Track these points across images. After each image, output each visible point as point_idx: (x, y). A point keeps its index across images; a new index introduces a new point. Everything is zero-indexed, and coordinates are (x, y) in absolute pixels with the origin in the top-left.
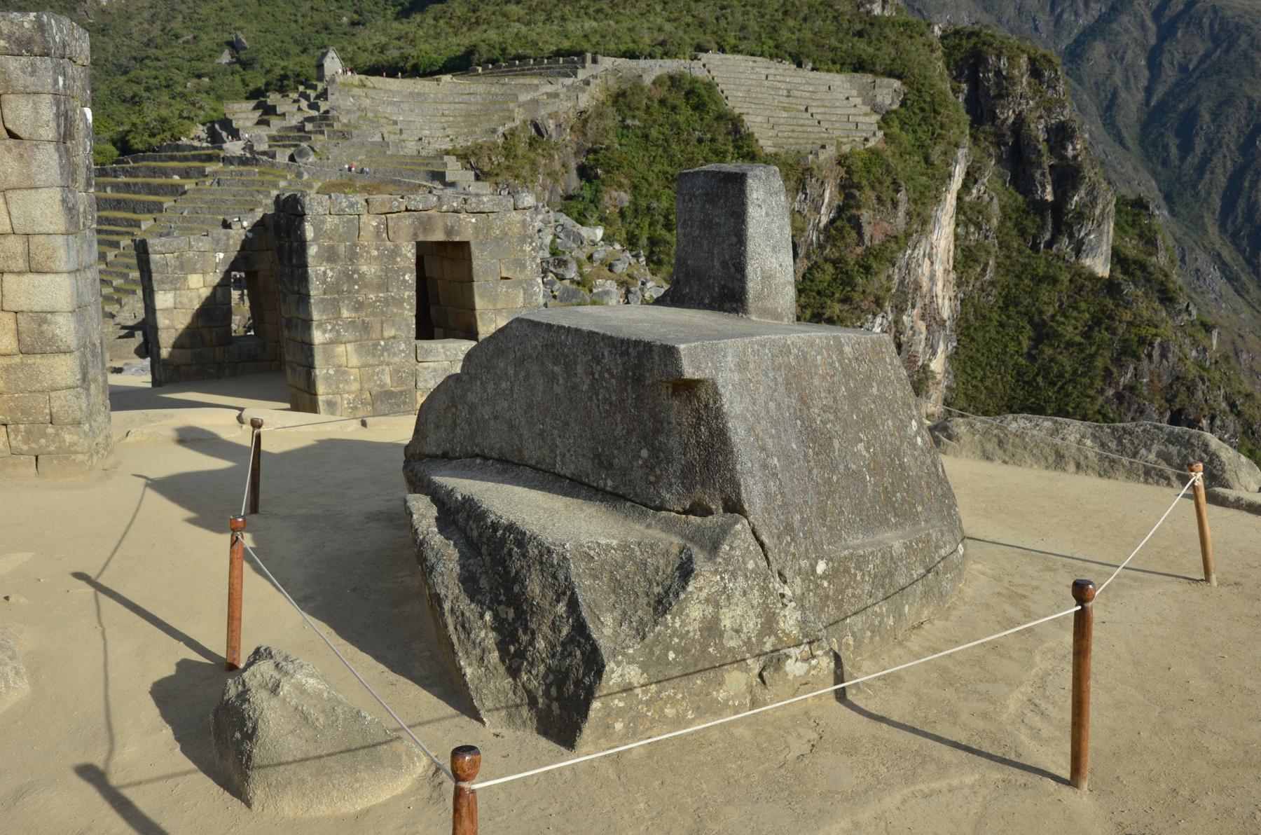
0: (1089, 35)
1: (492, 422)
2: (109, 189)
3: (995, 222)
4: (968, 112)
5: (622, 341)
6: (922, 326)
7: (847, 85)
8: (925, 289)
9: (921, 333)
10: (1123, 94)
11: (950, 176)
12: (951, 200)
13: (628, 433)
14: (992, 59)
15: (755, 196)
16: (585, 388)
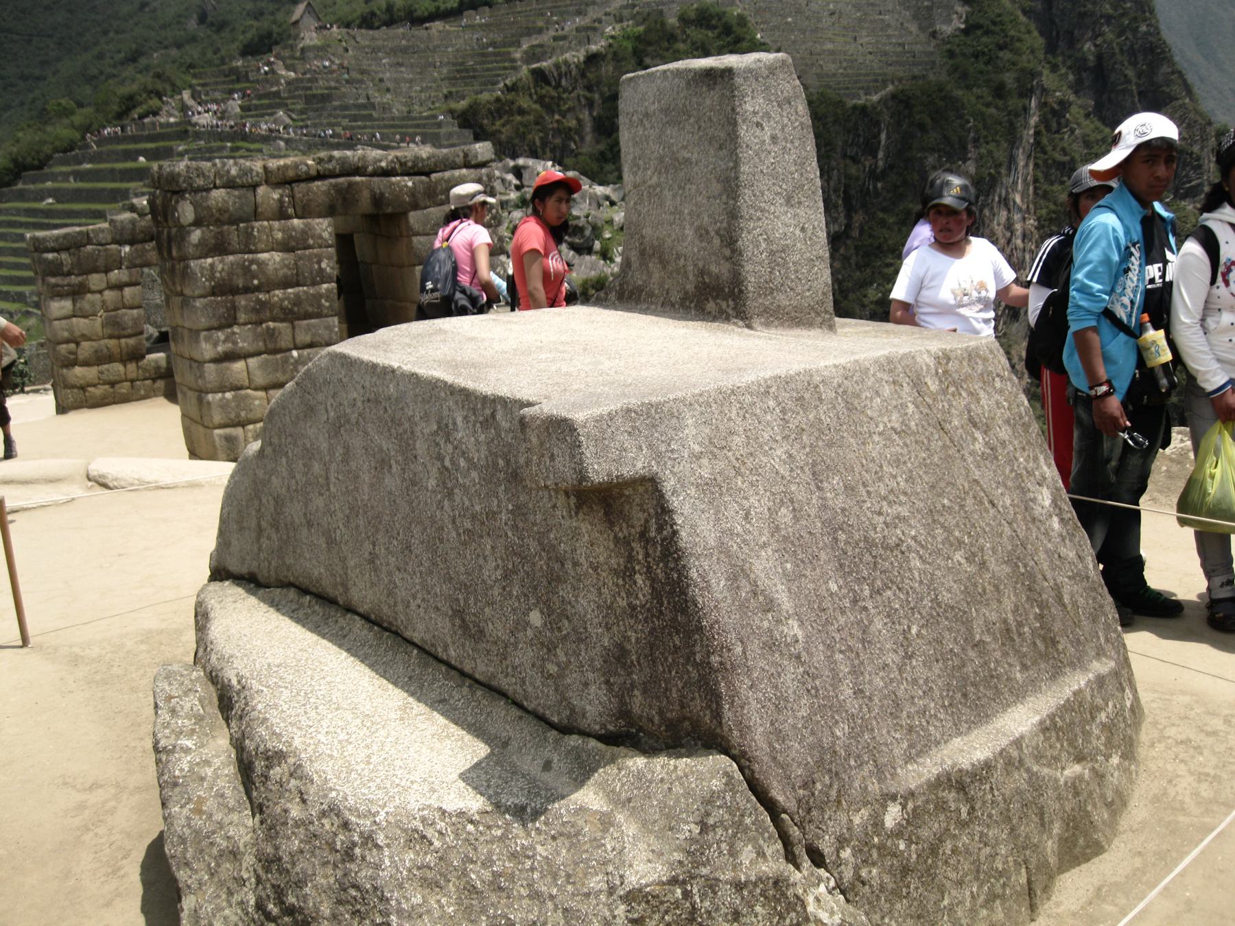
1: (305, 531)
2: (72, 179)
4: (1041, 34)
5: (485, 398)
13: (505, 577)
15: (748, 107)
16: (432, 483)
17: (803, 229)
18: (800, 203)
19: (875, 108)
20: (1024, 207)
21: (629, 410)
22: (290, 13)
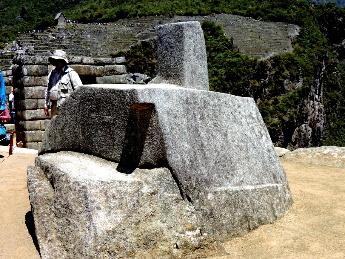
17: (201, 65)
18: (200, 59)
19: (266, 62)
20: (319, 100)
21: (149, 89)
22: (55, 16)
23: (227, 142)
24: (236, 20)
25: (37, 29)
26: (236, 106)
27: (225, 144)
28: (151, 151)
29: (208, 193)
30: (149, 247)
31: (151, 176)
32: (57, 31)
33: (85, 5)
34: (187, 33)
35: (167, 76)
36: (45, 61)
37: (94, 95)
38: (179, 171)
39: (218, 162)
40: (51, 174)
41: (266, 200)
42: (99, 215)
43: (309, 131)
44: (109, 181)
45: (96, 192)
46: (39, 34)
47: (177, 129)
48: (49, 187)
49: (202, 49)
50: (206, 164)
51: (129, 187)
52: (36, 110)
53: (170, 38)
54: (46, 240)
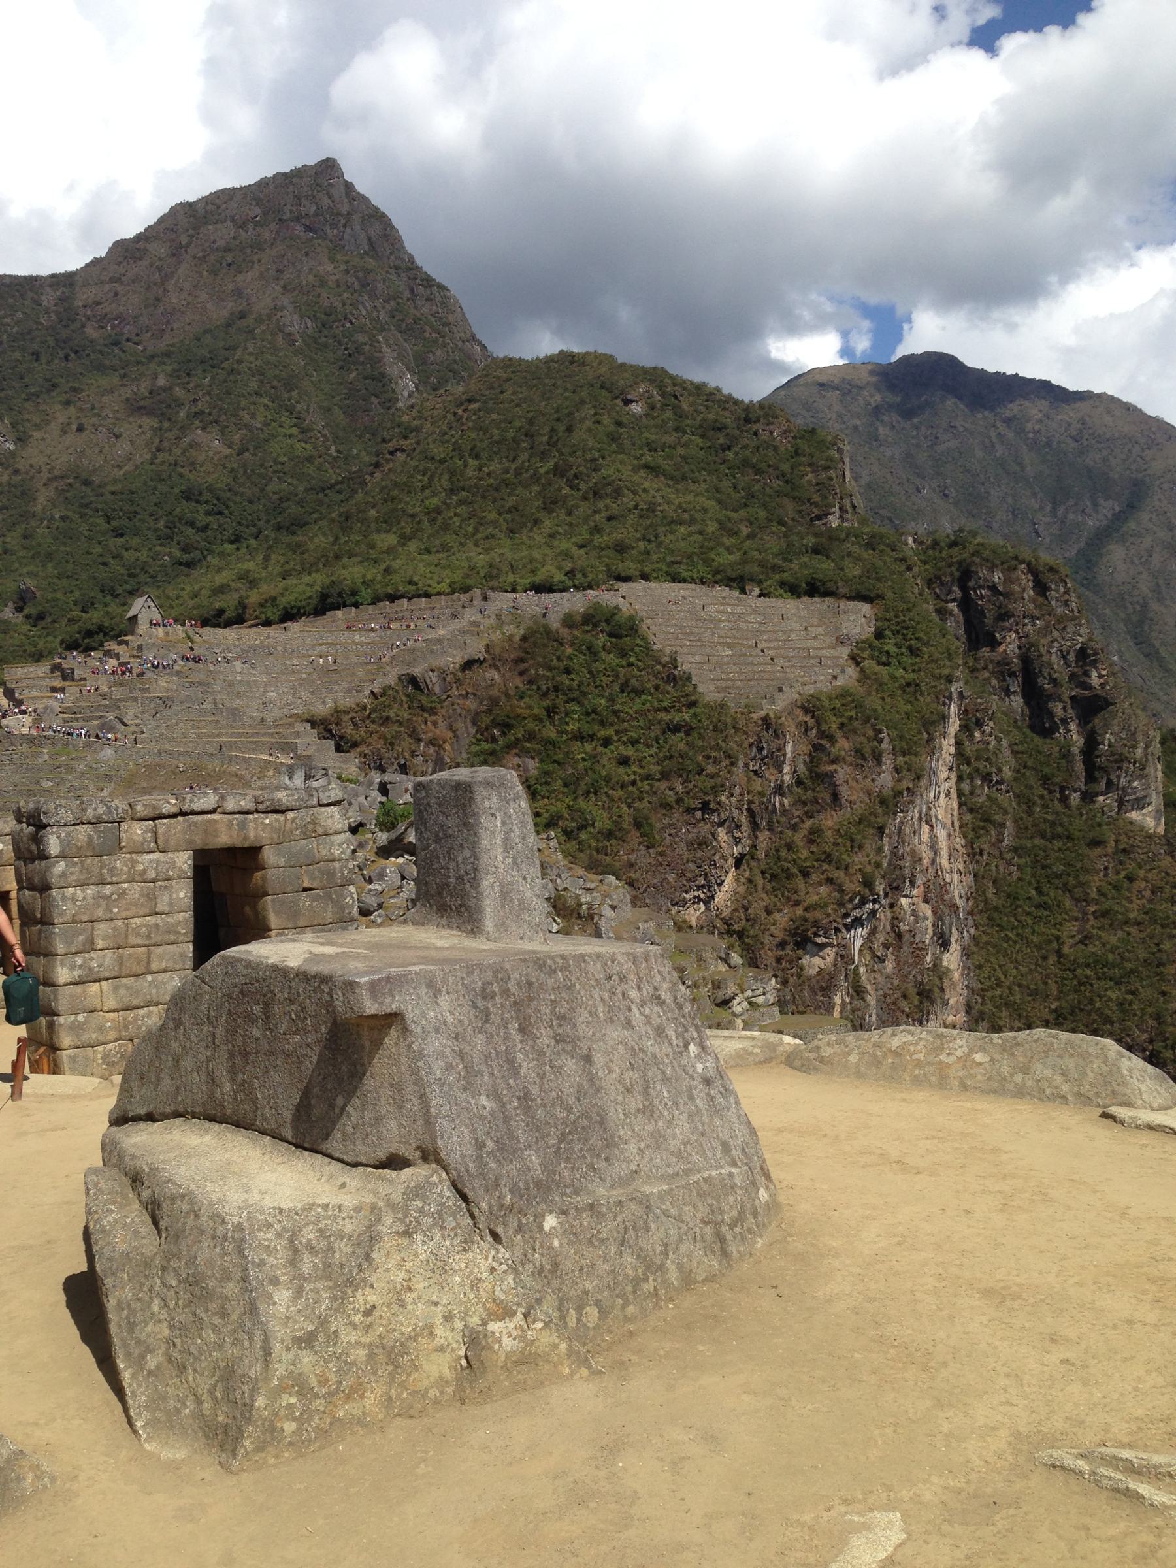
0: (1101, 537)
3: (1007, 773)
6: (926, 910)
7: (804, 613)
8: (926, 861)
9: (926, 918)
10: (1154, 606)
11: (944, 718)
12: (947, 746)
14: (983, 573)
17: (525, 878)
23: (592, 1080)
24: (684, 598)
25: (71, 646)
26: (615, 977)
27: (586, 1085)
28: (400, 1126)
29: (543, 1216)
30: (399, 1370)
31: (401, 1189)
32: (135, 653)
33: (219, 570)
34: (487, 801)
35: (442, 905)
36: (111, 812)
37: (258, 981)
38: (467, 1171)
39: (570, 1133)
40: (150, 1191)
41: (699, 1215)
42: (276, 1298)
43: (926, 918)
44: (300, 1206)
45: (267, 1240)
46: (74, 661)
47: (461, 1066)
48: (147, 1228)
49: (524, 839)
50: (537, 1141)
51: (347, 1220)
52: (86, 955)
53: (444, 814)
54: (142, 1370)
